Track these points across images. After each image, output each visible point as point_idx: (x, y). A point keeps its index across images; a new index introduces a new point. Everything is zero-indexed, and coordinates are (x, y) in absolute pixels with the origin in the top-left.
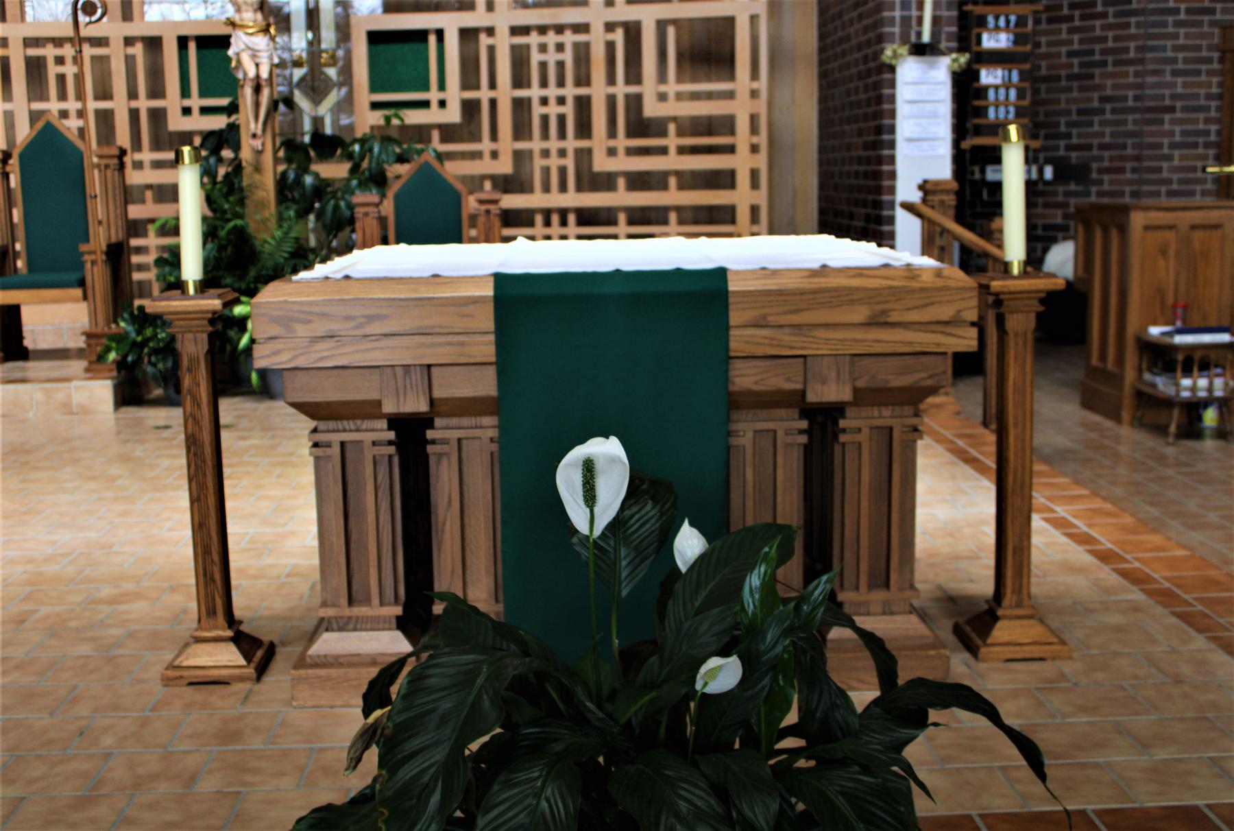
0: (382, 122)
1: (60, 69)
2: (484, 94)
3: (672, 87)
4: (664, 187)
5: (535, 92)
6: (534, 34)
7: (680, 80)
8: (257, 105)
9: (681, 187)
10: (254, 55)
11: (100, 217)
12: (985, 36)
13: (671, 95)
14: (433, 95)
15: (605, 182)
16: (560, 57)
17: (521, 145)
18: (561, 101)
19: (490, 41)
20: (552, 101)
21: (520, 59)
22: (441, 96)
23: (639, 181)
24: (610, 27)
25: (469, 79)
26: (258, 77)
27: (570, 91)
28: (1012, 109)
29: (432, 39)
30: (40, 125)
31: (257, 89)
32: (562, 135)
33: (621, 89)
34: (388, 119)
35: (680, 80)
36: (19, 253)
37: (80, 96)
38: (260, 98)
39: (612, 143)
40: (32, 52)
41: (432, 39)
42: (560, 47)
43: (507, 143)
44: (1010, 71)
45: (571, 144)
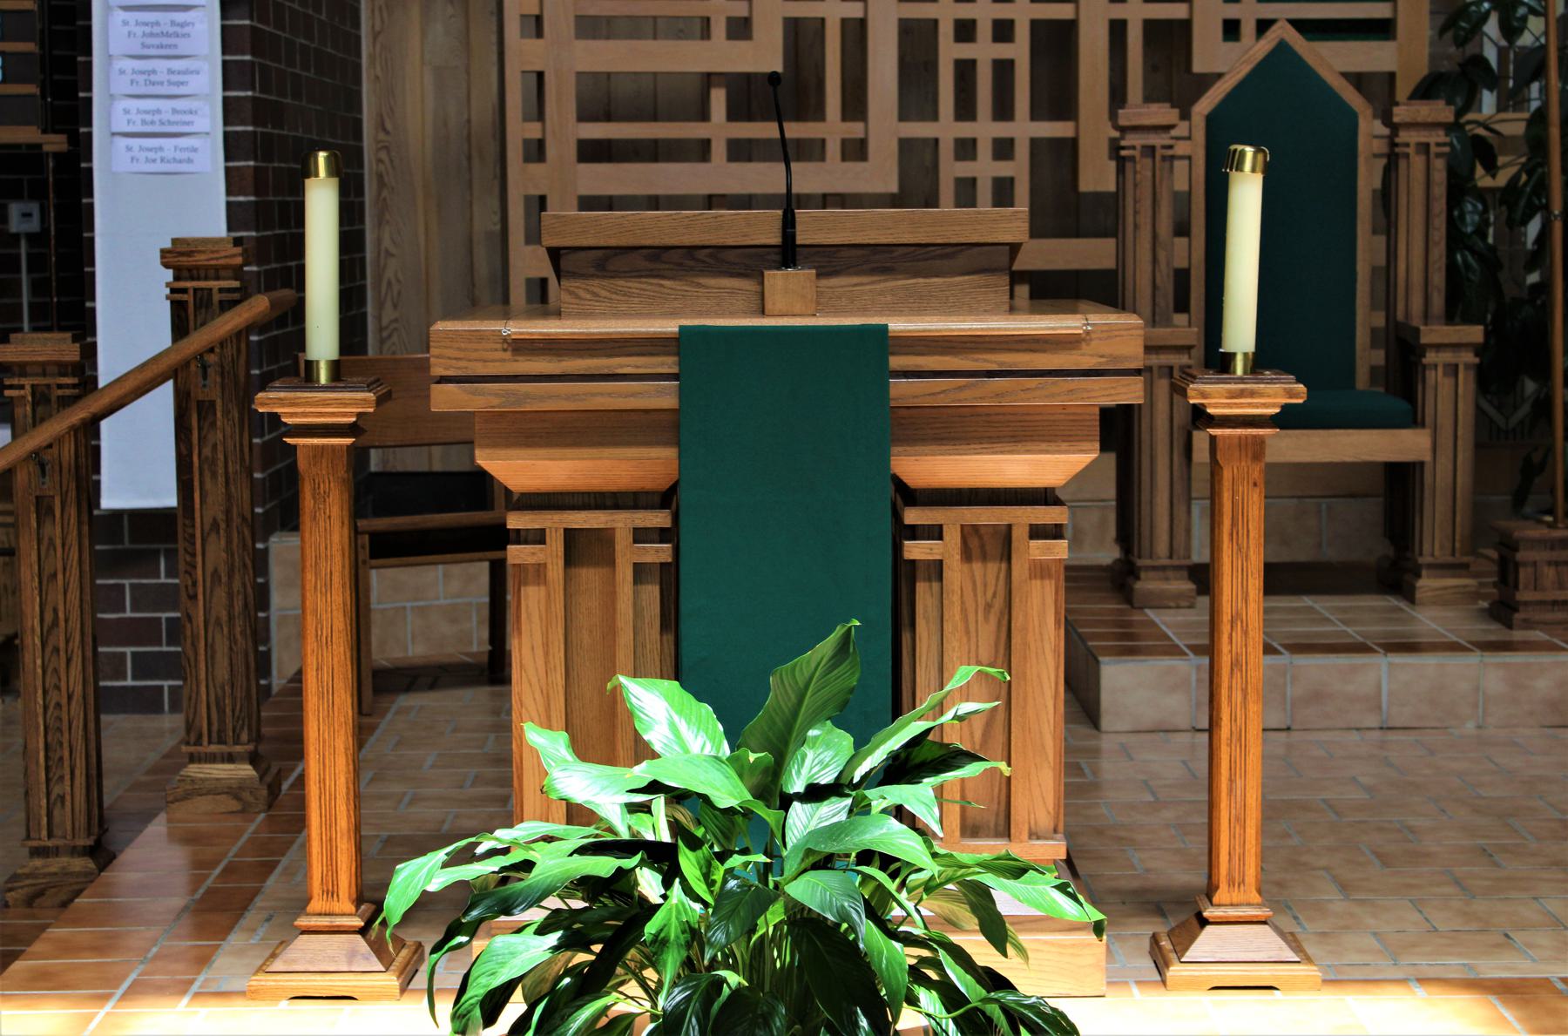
45: (1024, 128)
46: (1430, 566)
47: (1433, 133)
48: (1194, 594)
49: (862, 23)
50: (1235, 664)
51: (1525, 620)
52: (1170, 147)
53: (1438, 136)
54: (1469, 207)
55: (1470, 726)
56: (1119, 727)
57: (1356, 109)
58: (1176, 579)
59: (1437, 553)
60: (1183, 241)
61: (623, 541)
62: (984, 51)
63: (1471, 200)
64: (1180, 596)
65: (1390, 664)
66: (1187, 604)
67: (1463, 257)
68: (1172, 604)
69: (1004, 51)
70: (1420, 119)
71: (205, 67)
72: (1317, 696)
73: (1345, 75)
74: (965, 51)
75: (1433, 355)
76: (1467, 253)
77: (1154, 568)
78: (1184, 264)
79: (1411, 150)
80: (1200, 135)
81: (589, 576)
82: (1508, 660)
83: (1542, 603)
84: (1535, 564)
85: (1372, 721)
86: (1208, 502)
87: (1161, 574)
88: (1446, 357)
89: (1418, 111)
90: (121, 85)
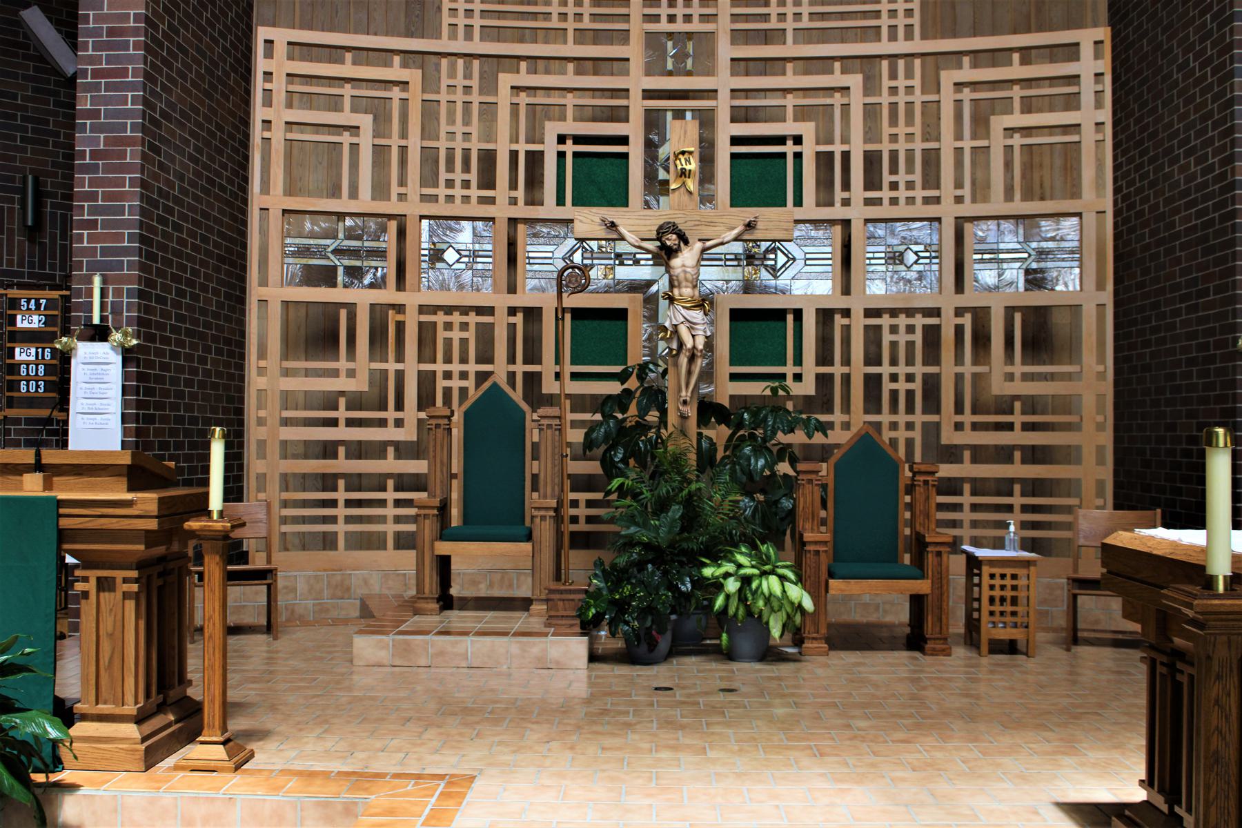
0: (768, 392)
1: (448, 334)
2: (837, 370)
3: (1018, 368)
4: (1009, 460)
5: (885, 369)
6: (886, 316)
7: (1024, 363)
8: (689, 373)
9: (975, 460)
10: (691, 326)
11: (454, 471)
12: (19, 318)
13: (1018, 375)
14: (789, 369)
15: (952, 454)
16: (910, 337)
17: (934, 418)
18: (910, 378)
19: (845, 321)
20: (902, 378)
21: (873, 335)
22: (797, 370)
23: (980, 454)
24: (959, 312)
25: (824, 358)
26: (694, 347)
27: (919, 369)
28: (42, 383)
29: (790, 318)
30: (487, 385)
31: (692, 359)
32: (910, 409)
33: (968, 369)
34: (774, 390)
35: (1024, 363)
36: (906, 510)
37: (464, 360)
38: (693, 367)
39: (959, 418)
40: (424, 318)
41: (790, 318)
42: (910, 329)
43: (859, 418)
44: (43, 349)
45: (919, 418)
50: (210, 637)
55: (505, 667)
56: (360, 664)
61: (119, 581)
62: (902, 386)
64: (432, 610)
71: (114, 386)
72: (441, 653)
74: (894, 386)
81: (105, 596)
83: (557, 616)
85: (464, 664)
90: (80, 394)
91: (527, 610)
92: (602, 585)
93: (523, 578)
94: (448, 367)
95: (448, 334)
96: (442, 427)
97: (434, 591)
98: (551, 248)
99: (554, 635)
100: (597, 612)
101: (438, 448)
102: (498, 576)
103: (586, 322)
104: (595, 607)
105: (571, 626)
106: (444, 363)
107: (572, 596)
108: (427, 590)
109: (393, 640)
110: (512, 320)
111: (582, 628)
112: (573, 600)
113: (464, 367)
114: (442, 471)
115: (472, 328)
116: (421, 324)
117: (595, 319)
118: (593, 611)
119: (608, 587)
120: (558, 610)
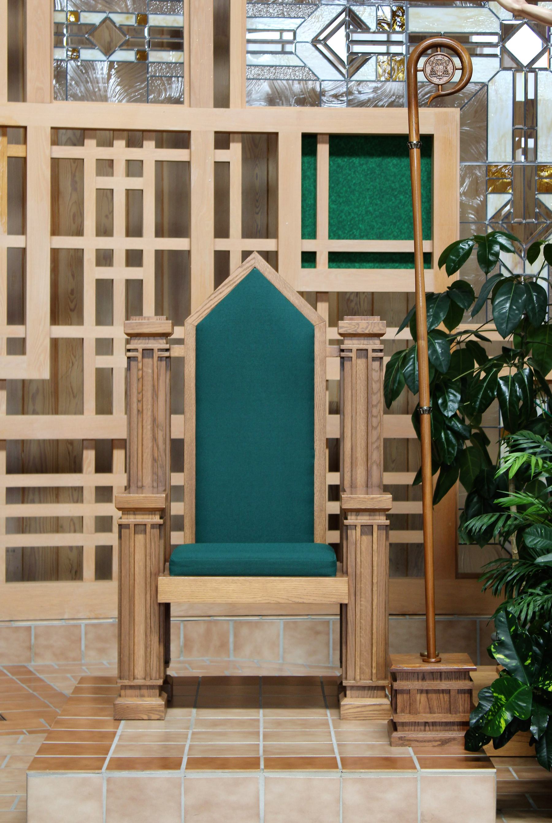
20: (120, 258)
46: (352, 688)
47: (371, 342)
48: (163, 709)
49: (24, 251)
51: (401, 738)
52: (167, 350)
53: (375, 344)
54: (452, 397)
57: (313, 322)
58: (150, 696)
59: (358, 677)
60: (336, 418)
63: (453, 391)
64: (151, 710)
65: (266, 778)
66: (158, 717)
67: (446, 435)
68: (145, 717)
69: (134, 273)
70: (359, 331)
73: (302, 294)
75: (353, 517)
76: (449, 432)
77: (132, 687)
78: (336, 435)
79: (353, 355)
80: (191, 342)
82: (363, 776)
83: (416, 724)
84: (408, 692)
86: (339, 617)
87: (137, 692)
88: (364, 519)
89: (358, 324)
91: (336, 705)
92: (514, 663)
93: (245, 631)
94: (104, 243)
95: (105, 182)
96: (156, 354)
97: (154, 674)
98: (291, 24)
99: (426, 764)
100: (515, 719)
101: (148, 394)
102: (201, 629)
103: (356, 161)
104: (510, 708)
105: (444, 742)
106: (128, 234)
107: (444, 685)
108: (139, 671)
109: (109, 780)
110: (222, 155)
111: (467, 748)
112: (448, 692)
113: (134, 243)
114: (154, 439)
115: (149, 170)
116: (55, 163)
117: (371, 155)
118: (507, 716)
119: (526, 668)
120: (417, 713)
